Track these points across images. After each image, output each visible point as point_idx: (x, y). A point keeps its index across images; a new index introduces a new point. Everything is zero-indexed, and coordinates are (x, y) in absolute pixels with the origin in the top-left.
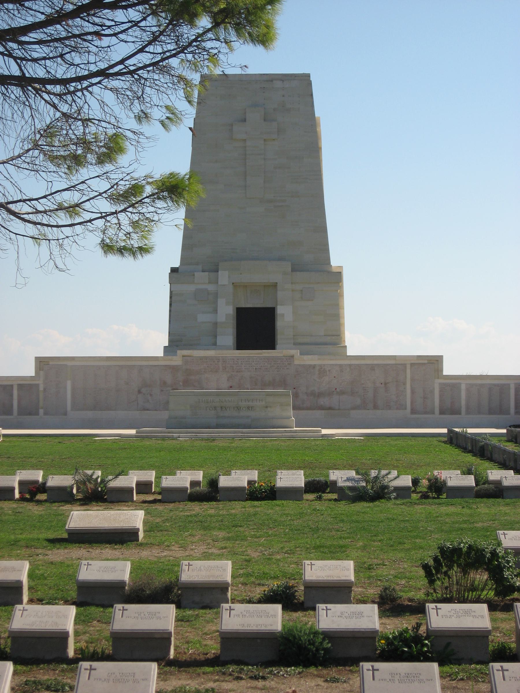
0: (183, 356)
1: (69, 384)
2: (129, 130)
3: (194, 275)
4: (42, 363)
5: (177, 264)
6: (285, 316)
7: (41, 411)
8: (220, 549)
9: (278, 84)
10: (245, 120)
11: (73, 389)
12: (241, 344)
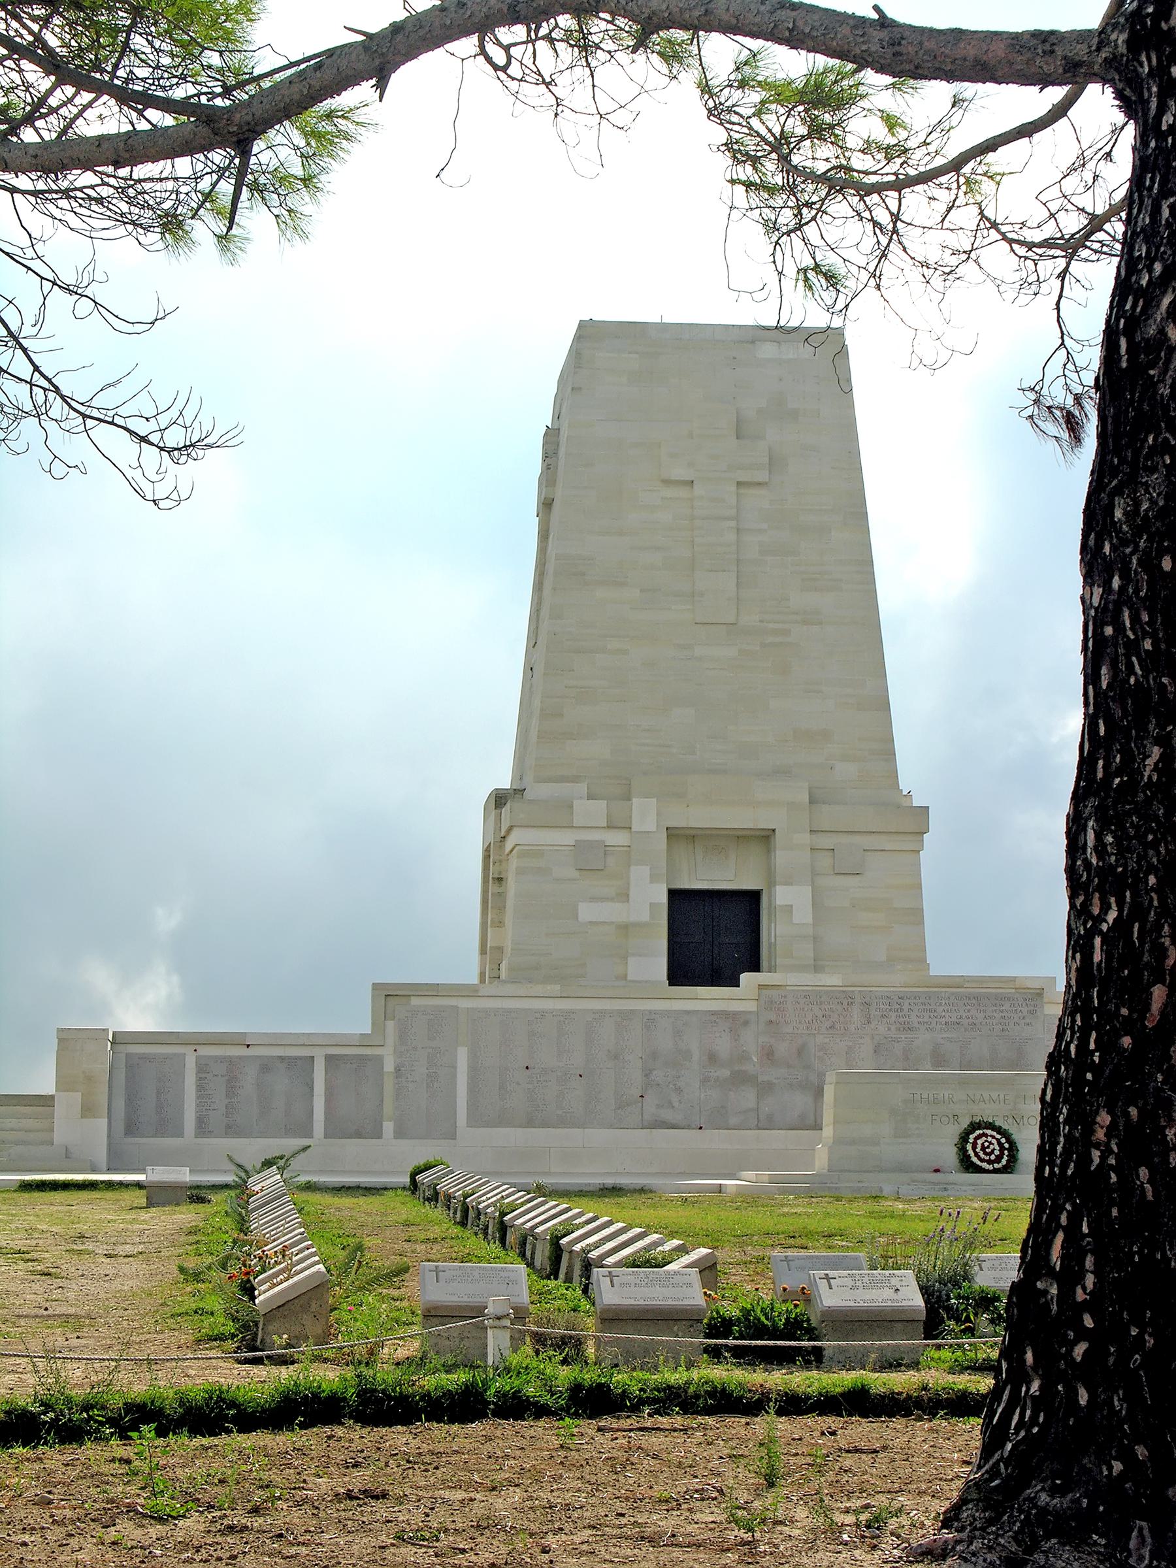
0: (761, 987)
1: (462, 1057)
2: (119, 381)
3: (571, 807)
4: (389, 996)
6: (788, 914)
7: (388, 1127)
8: (951, 1371)
12: (681, 972)
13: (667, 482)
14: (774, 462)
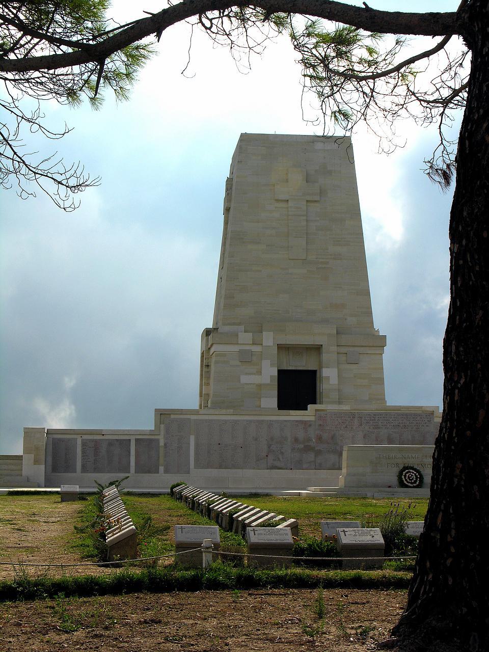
4: (162, 415)
5: (210, 325)
6: (329, 377)
7: (161, 469)
9: (319, 146)
10: (287, 181)
11: (197, 445)
13: (277, 201)
14: (322, 192)
